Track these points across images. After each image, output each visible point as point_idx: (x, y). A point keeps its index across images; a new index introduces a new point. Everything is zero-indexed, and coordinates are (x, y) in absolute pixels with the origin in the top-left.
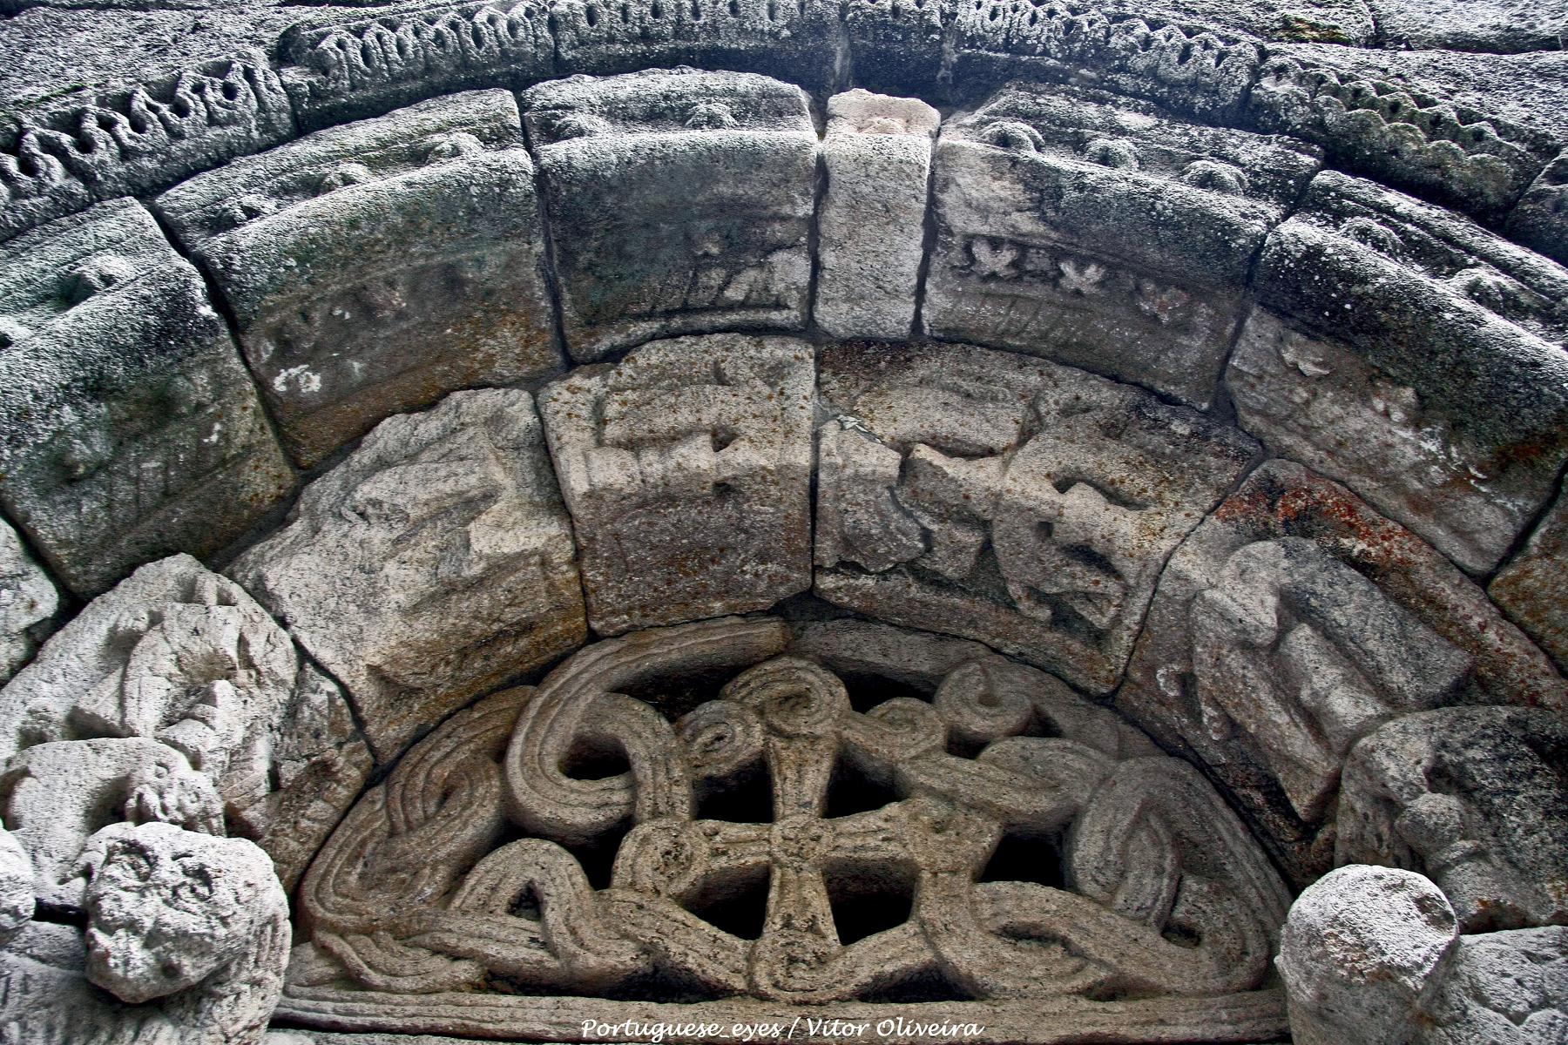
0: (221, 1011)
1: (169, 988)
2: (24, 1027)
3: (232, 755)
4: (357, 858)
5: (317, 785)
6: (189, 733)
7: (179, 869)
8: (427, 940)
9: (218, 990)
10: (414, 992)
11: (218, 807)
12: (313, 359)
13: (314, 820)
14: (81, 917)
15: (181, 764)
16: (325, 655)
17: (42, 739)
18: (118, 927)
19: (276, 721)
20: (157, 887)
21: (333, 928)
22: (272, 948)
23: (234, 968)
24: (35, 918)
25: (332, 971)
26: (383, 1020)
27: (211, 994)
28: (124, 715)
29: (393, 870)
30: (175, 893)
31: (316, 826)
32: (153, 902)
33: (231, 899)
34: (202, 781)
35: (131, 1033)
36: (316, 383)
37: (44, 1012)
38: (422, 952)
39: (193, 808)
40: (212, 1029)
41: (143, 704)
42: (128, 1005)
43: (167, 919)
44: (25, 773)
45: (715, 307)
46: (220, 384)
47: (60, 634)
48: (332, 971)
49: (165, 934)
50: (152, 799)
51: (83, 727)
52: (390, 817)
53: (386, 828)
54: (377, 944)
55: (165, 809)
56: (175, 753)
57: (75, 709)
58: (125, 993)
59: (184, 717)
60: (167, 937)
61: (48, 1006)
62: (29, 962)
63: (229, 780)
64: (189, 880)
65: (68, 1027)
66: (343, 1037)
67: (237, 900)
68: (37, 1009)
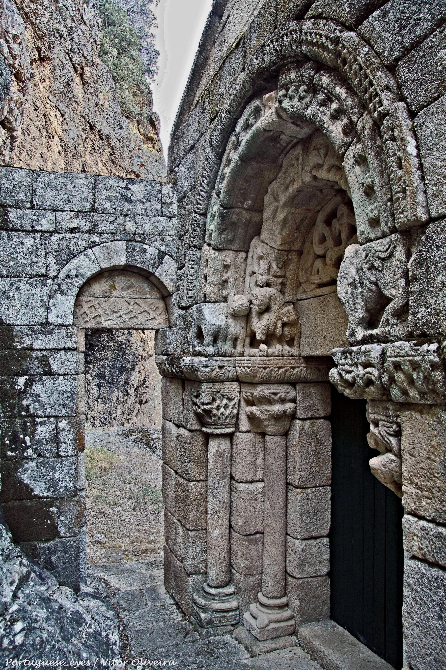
12: (245, 200)
16: (274, 246)
36: (250, 202)
45: (285, 147)
46: (238, 214)
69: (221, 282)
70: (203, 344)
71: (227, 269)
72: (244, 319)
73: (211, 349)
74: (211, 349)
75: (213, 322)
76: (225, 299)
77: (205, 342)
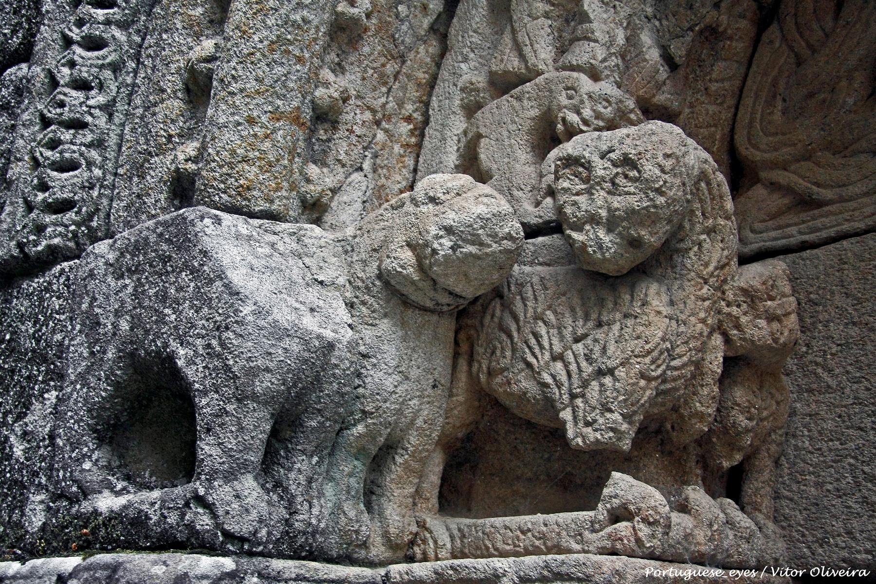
0: (691, 260)
1: (640, 257)
2: (555, 313)
3: (623, 57)
4: (774, 97)
5: (712, 49)
6: (581, 54)
7: (608, 164)
8: (864, 144)
9: (682, 245)
10: (866, 194)
11: (631, 104)
13: (722, 80)
14: (554, 227)
15: (586, 83)
17: (479, 106)
18: (584, 224)
19: (649, 10)
20: (598, 184)
21: (774, 165)
22: (713, 199)
23: (687, 226)
24: (527, 237)
25: (786, 201)
26: (846, 227)
27: (678, 251)
28: (526, 62)
29: (811, 95)
30: (614, 184)
31: (727, 85)
32: (600, 196)
33: (657, 172)
34: (606, 87)
35: (628, 297)
37: (564, 298)
38: (863, 157)
39: (608, 112)
40: (689, 277)
41: (536, 46)
42: (617, 277)
43: (616, 205)
44: (479, 136)
47: (455, 20)
48: (786, 201)
49: (619, 217)
50: (573, 118)
51: (503, 84)
52: (791, 48)
53: (792, 60)
54: (818, 164)
55: (586, 122)
56: (575, 74)
57: (490, 72)
58: (610, 269)
59: (572, 42)
60: (623, 219)
61: (564, 294)
62: (539, 268)
63: (631, 78)
64: (619, 170)
65: (583, 304)
66: (815, 251)
67: (663, 171)
68: (558, 298)
69: (307, 114)
70: (186, 465)
71: (343, 54)
72: (447, 327)
73: (245, 502)
74: (245, 502)
75: (283, 316)
76: (315, 210)
77: (207, 448)
